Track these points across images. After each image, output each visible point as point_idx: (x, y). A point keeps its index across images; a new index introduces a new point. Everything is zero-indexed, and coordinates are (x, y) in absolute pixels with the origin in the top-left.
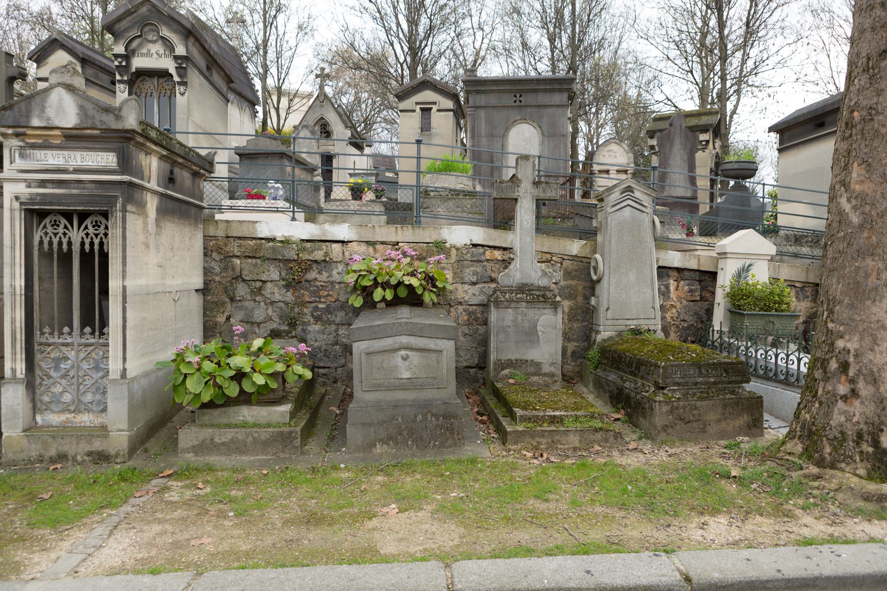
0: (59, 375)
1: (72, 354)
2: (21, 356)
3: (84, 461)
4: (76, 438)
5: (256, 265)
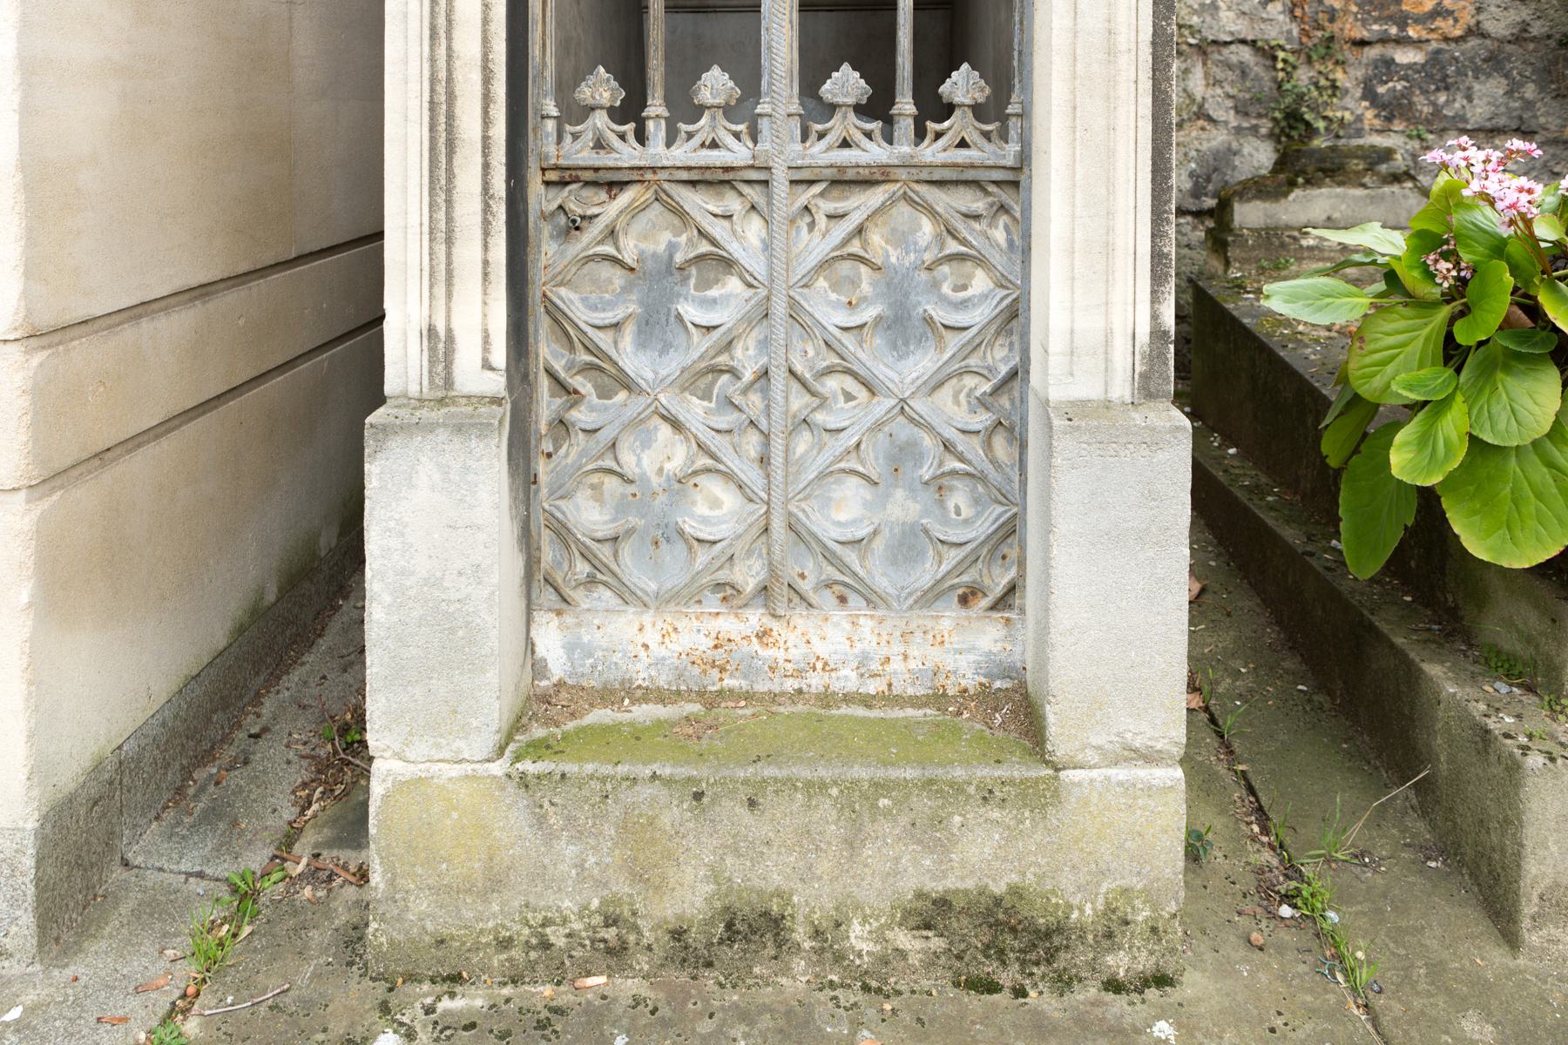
0: (673, 364)
1: (746, 239)
2: (480, 251)
4: (845, 806)
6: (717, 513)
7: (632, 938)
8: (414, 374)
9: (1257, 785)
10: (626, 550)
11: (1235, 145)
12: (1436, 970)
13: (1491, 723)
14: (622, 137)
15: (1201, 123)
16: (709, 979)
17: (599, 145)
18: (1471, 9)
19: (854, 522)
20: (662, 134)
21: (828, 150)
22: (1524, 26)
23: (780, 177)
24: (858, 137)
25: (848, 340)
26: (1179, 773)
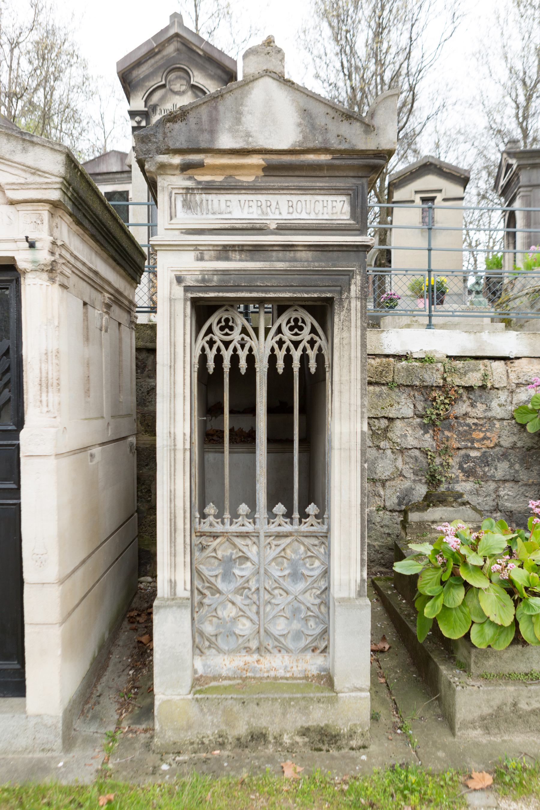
0: (232, 587)
1: (252, 552)
2: (183, 558)
3: (294, 744)
5: (380, 395)
6: (245, 628)
7: (226, 741)
8: (166, 592)
9: (397, 702)
10: (219, 638)
11: (413, 486)
12: (434, 743)
13: (452, 680)
14: (218, 523)
15: (401, 478)
16: (247, 751)
17: (211, 525)
18: (497, 437)
19: (283, 630)
20: (229, 523)
21: (275, 527)
22: (515, 443)
23: (262, 535)
24: (283, 523)
25: (281, 580)
26: (369, 694)
